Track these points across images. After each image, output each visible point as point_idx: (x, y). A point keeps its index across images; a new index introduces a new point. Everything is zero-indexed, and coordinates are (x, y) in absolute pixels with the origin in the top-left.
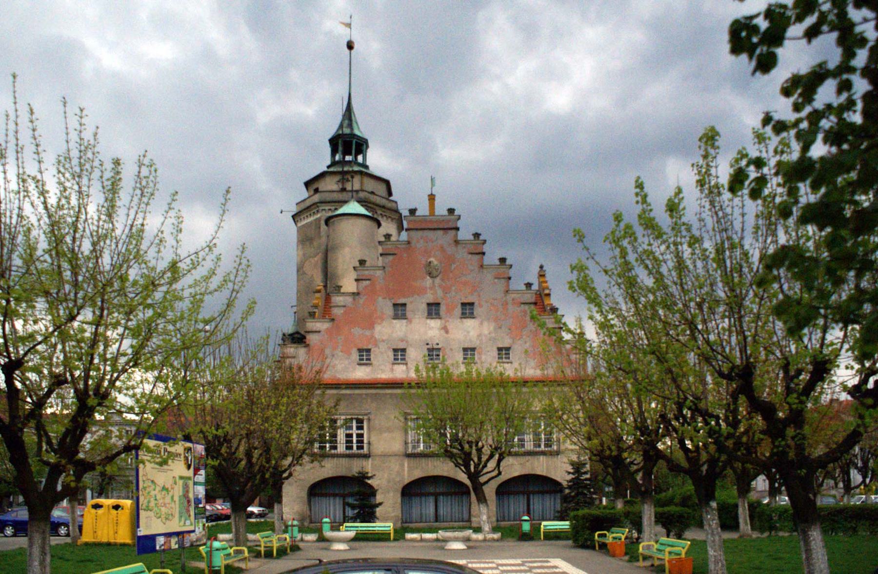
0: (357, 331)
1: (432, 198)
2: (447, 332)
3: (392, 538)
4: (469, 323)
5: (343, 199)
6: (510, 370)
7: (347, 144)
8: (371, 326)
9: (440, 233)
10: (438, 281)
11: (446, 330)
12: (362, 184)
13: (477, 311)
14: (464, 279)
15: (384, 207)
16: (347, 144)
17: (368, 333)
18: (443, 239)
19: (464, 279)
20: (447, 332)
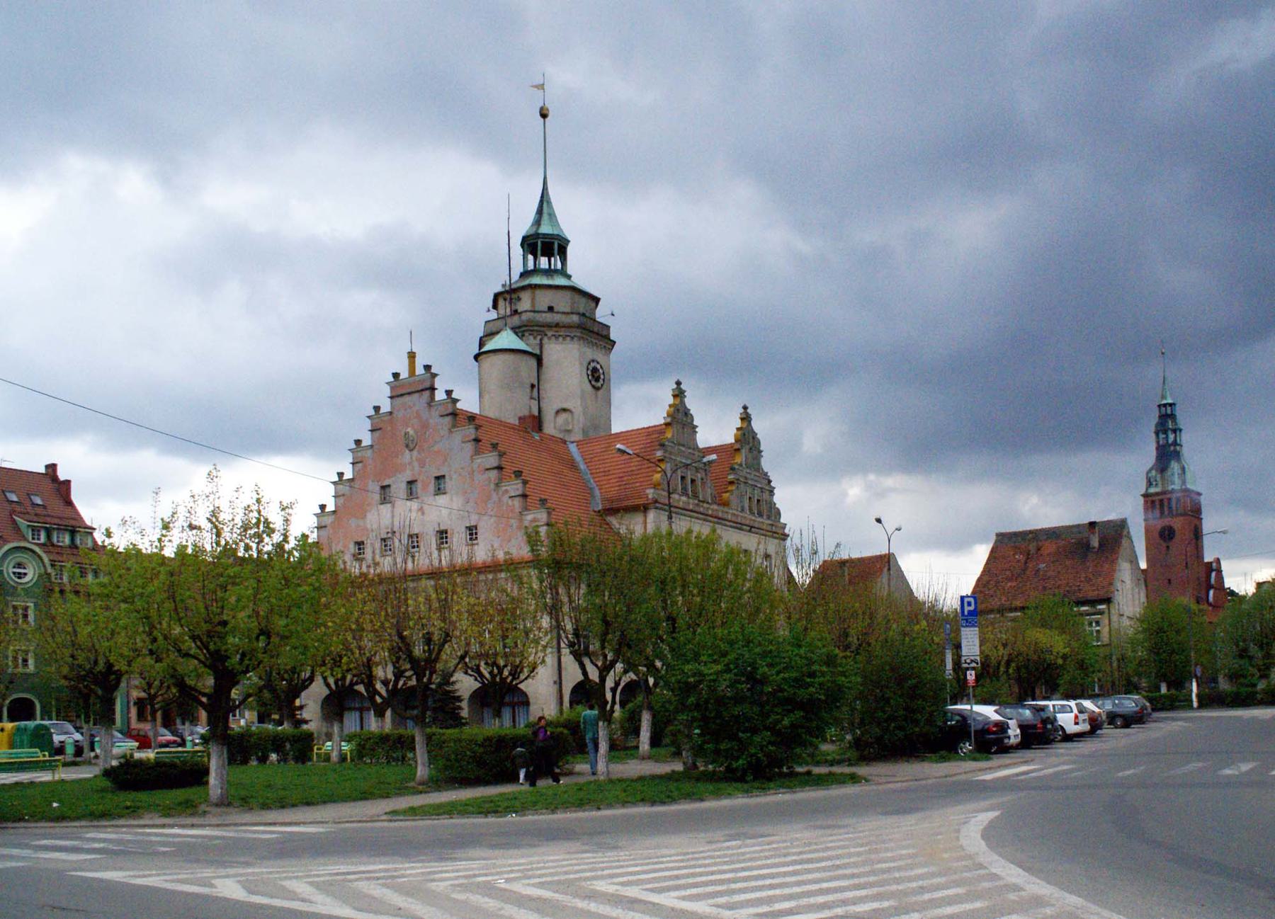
0: (353, 522)
1: (412, 356)
2: (423, 513)
3: (1195, 704)
4: (442, 500)
5: (494, 330)
6: (481, 554)
7: (545, 244)
8: (364, 517)
9: (416, 395)
10: (415, 453)
11: (421, 510)
12: (533, 300)
13: (449, 484)
14: (435, 448)
15: (557, 325)
16: (545, 244)
17: (361, 523)
18: (419, 402)
19: (435, 448)
20: (423, 513)
